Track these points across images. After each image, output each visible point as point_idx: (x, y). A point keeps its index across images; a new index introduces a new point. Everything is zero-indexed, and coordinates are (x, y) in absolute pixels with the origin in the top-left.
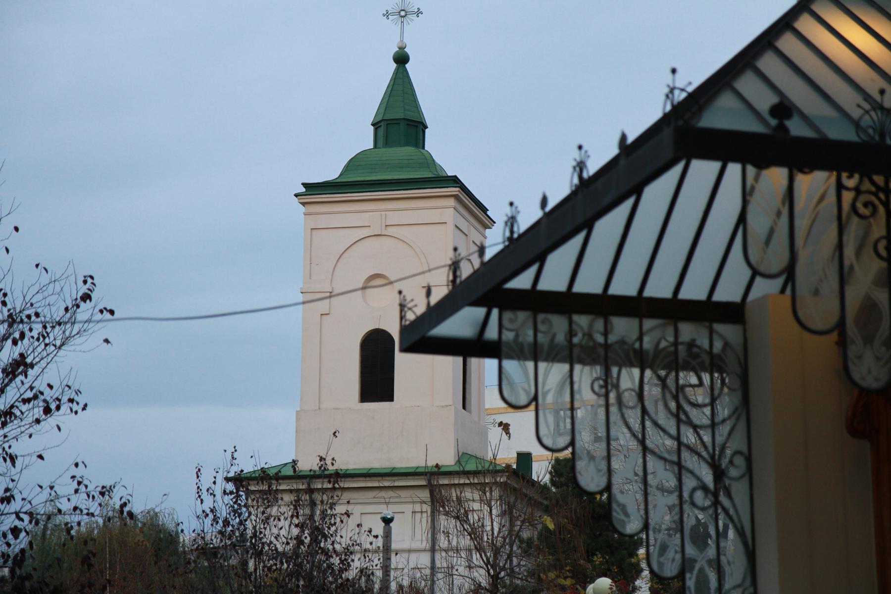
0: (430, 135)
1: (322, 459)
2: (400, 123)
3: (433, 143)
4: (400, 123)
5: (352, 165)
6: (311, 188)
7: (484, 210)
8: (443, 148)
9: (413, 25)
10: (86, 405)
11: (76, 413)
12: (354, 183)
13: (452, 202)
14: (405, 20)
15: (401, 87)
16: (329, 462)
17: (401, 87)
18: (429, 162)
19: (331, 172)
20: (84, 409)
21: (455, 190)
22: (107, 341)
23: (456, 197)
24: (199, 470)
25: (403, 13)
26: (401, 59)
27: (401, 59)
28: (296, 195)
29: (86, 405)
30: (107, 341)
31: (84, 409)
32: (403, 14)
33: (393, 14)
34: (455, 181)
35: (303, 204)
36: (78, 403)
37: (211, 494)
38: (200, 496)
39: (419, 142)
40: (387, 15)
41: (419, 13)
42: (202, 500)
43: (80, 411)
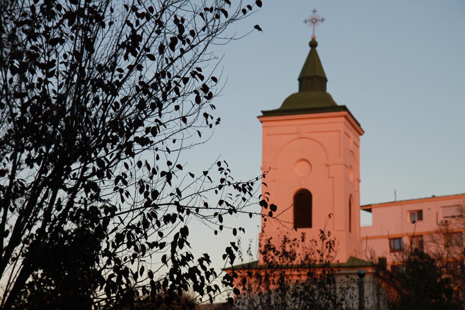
0: (328, 84)
1: (322, 232)
2: (312, 76)
3: (330, 89)
4: (312, 76)
5: (288, 101)
6: (266, 114)
7: (359, 125)
8: (336, 91)
9: (320, 27)
10: (219, 119)
11: (211, 126)
12: (290, 108)
13: (343, 119)
14: (315, 24)
15: (313, 61)
16: (326, 233)
17: (313, 61)
18: (329, 97)
19: (277, 105)
20: (217, 123)
21: (344, 113)
22: (257, 27)
23: (346, 117)
24: (239, 240)
25: (314, 21)
26: (313, 44)
27: (313, 44)
28: (258, 117)
29: (219, 119)
30: (257, 27)
31: (217, 123)
32: (314, 21)
33: (309, 21)
34: (344, 108)
35: (262, 122)
36: (212, 118)
37: (250, 254)
38: (240, 257)
39: (324, 87)
40: (305, 22)
41: (323, 20)
42: (242, 259)
43: (214, 125)
